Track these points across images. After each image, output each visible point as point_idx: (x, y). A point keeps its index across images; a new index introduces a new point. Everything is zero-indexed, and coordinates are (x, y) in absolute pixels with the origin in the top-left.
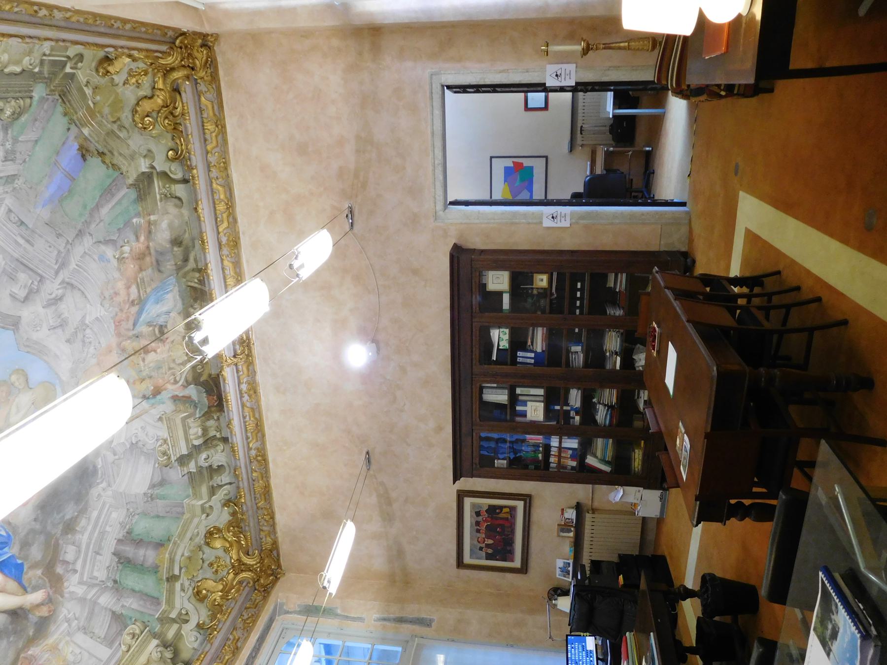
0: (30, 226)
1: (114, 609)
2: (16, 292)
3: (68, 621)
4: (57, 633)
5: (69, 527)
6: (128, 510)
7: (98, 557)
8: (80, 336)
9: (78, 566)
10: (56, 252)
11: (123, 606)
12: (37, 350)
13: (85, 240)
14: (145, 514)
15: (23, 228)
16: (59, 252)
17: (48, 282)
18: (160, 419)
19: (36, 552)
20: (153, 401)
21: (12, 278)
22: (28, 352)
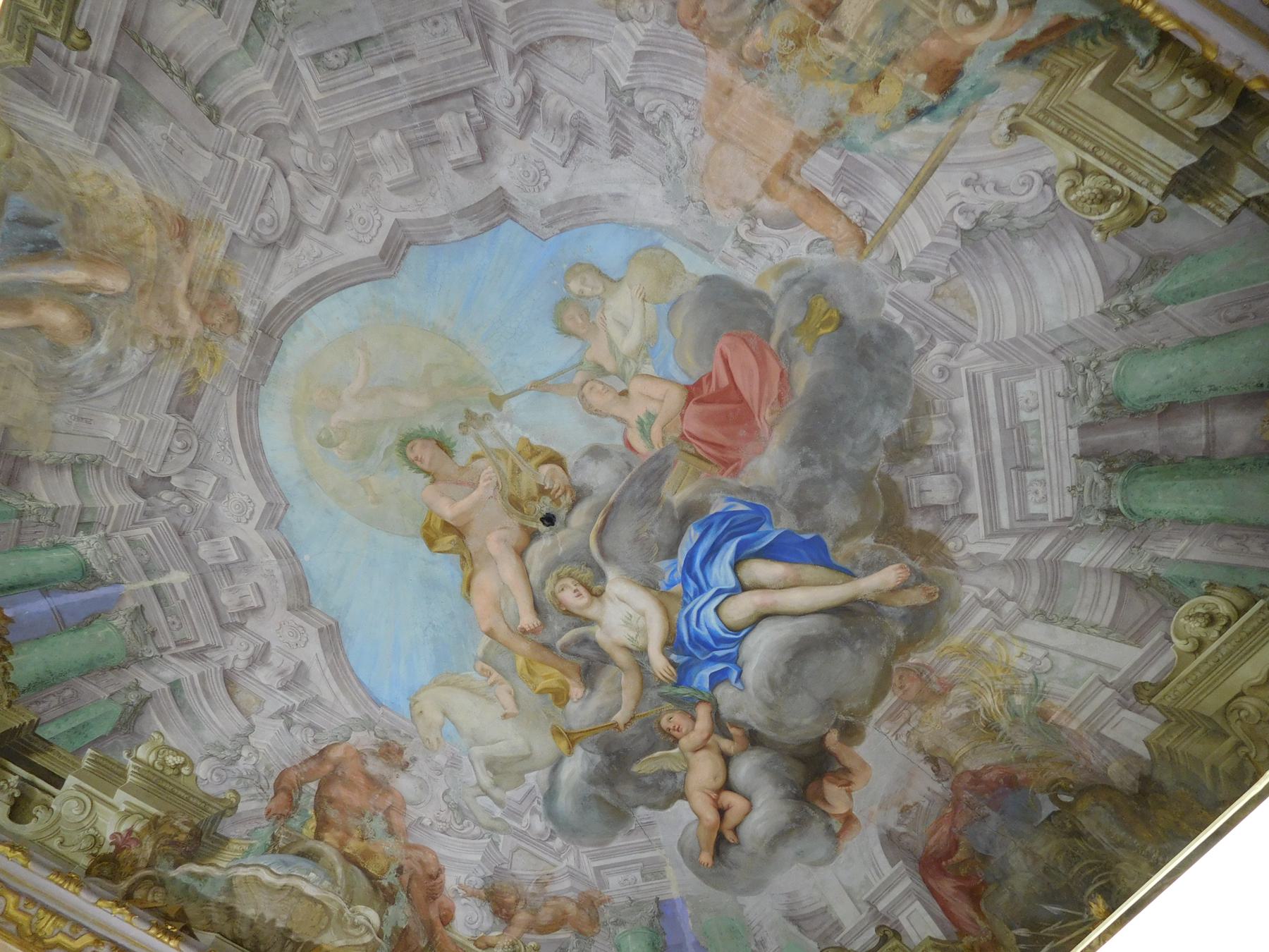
0: (377, 28)
1: (1126, 568)
2: (459, 156)
3: (989, 604)
4: (968, 625)
5: (906, 447)
6: (1067, 363)
7: (1029, 476)
8: (632, 123)
10: (452, 21)
11: (1155, 559)
12: (575, 213)
14: (1141, 351)
15: (368, 49)
17: (488, 87)
18: (1015, 130)
19: (840, 511)
20: (953, 105)
21: (435, 141)
22: (562, 231)
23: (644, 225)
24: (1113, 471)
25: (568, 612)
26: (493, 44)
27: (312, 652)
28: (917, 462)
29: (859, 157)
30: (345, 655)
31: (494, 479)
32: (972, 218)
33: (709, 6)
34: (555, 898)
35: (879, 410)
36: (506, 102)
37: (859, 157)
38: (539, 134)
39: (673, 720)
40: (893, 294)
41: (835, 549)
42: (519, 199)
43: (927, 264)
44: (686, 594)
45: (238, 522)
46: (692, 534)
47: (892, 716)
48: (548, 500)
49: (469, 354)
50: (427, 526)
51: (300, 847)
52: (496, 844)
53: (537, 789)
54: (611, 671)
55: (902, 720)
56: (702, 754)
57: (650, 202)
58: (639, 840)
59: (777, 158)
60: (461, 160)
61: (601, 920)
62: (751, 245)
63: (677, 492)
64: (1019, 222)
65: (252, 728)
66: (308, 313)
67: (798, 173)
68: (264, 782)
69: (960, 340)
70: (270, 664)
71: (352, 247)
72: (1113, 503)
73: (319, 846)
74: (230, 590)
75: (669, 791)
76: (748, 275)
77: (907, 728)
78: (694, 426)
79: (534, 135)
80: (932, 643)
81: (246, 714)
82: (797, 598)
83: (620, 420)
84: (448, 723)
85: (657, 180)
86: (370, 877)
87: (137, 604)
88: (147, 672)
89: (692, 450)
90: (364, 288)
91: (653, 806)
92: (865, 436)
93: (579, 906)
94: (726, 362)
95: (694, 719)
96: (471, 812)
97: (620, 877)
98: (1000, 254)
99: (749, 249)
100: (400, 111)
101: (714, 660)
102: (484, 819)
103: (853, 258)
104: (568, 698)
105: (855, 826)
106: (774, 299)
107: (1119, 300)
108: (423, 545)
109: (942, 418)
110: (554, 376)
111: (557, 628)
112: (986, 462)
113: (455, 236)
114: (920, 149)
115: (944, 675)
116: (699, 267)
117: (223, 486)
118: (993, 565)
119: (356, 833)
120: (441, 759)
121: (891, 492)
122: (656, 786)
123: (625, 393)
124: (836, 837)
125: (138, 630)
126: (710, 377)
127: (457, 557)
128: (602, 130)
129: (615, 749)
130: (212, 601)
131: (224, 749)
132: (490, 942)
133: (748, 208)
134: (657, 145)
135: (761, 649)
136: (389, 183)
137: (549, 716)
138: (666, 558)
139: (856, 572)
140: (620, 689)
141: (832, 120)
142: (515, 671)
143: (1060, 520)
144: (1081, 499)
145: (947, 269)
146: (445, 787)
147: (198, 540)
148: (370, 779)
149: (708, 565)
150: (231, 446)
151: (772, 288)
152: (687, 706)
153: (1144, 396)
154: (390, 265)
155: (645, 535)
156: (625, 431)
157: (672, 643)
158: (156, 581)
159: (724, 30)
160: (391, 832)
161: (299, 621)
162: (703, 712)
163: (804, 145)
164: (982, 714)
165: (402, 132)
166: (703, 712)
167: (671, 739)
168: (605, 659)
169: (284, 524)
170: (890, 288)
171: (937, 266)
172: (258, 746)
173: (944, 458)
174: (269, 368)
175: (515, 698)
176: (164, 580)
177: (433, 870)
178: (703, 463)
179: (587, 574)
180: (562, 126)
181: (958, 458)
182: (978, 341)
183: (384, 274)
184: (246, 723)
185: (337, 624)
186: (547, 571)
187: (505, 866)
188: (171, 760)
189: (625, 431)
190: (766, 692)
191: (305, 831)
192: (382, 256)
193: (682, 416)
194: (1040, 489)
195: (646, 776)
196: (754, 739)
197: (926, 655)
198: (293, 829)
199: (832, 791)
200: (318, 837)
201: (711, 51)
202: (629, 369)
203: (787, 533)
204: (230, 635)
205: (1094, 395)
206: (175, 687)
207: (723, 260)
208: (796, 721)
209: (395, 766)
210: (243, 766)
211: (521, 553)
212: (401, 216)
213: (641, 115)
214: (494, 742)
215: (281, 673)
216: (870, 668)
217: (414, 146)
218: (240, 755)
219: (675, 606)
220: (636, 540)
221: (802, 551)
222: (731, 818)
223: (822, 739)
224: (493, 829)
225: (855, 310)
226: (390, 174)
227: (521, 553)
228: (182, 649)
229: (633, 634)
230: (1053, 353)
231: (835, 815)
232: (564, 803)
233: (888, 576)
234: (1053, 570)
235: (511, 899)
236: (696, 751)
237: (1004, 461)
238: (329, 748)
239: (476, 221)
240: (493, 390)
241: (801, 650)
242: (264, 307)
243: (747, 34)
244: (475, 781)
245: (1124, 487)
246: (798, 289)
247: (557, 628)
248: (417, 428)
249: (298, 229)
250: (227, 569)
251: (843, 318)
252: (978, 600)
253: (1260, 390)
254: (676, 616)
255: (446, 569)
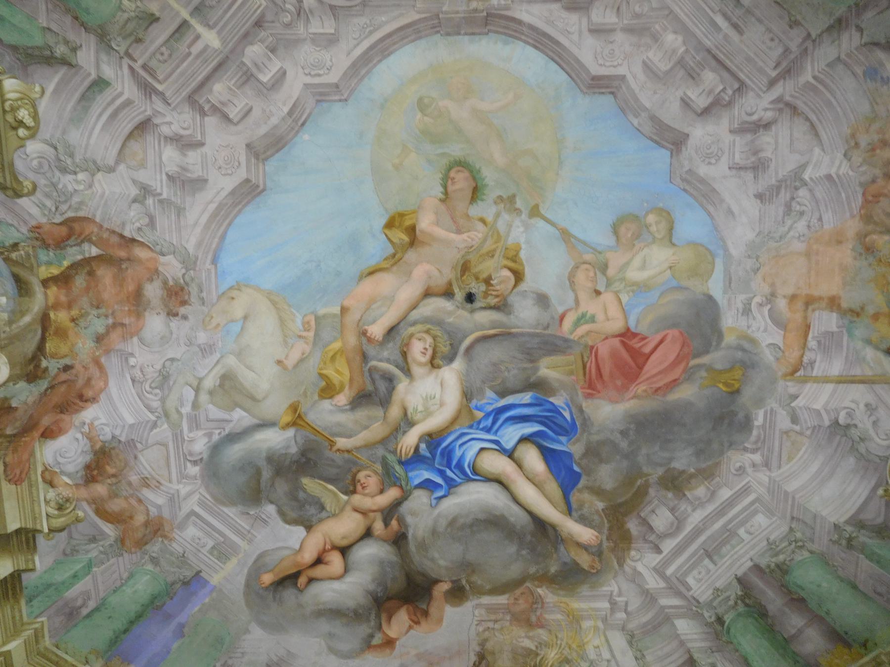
2: (693, 97)
3: (613, 604)
4: (588, 603)
5: (675, 483)
6: (791, 530)
7: (707, 561)
8: (784, 196)
9: (668, 546)
10: (780, 50)
12: (703, 193)
13: (845, 37)
14: (824, 560)
16: (787, 50)
17: (751, 94)
19: (607, 475)
21: (693, 76)
22: (685, 190)
23: (722, 239)
24: (743, 601)
25: (404, 355)
26: (781, 83)
27: (223, 184)
28: (670, 495)
29: (845, 338)
30: (240, 211)
31: (474, 243)
32: (849, 421)
33: (884, 202)
34: (140, 501)
35: (690, 451)
36: (749, 110)
37: (845, 338)
38: (740, 141)
39: (369, 479)
40: (772, 410)
41: (580, 491)
42: (689, 151)
43: (804, 416)
44: (479, 422)
45: (299, 71)
46: (526, 397)
47: (490, 609)
48: (483, 288)
49: (557, 174)
50: (402, 215)
51: (23, 273)
52: (155, 425)
53: (231, 425)
54: (379, 412)
55: (493, 617)
56: (358, 516)
57: (740, 234)
58: (244, 523)
59: (816, 293)
60: (692, 101)
61: (147, 547)
62: (750, 310)
63: (548, 369)
64: (862, 448)
65: (111, 170)
66: (521, 44)
67: (814, 310)
68: (64, 207)
69: (767, 464)
70: (185, 155)
71: (589, 53)
72: (726, 618)
73: (38, 289)
74: (230, 89)
75: (304, 514)
76: (730, 321)
77: (490, 625)
78: (604, 350)
79: (738, 139)
80: (562, 593)
81: (121, 156)
82: (528, 493)
83: (577, 302)
84: (240, 324)
85: (758, 230)
86: (41, 348)
87: (157, 14)
88: (97, 52)
89: (586, 359)
90: (564, 76)
91: (282, 513)
92: (666, 455)
93: (146, 524)
94: (661, 342)
95: (382, 492)
96: (170, 389)
97: (199, 534)
98: (836, 450)
99: (747, 311)
100: (700, 43)
101: (442, 473)
102: (171, 404)
103: (780, 374)
104: (331, 397)
105: (388, 651)
106: (723, 344)
107: (849, 529)
108: (383, 221)
109: (708, 489)
110: (579, 240)
111: (385, 354)
112: (697, 532)
113: (635, 122)
114: (871, 368)
115: (547, 616)
116: (715, 287)
117: (331, 41)
118: (639, 586)
119: (75, 312)
120: (202, 337)
121: (641, 494)
122: (302, 505)
123: (598, 293)
124: (368, 645)
125: (131, 26)
126: (644, 338)
127: (391, 250)
128: (769, 179)
129: (311, 456)
130: (208, 78)
131: (72, 156)
132: (56, 481)
133: (773, 295)
134: (780, 218)
135: (475, 496)
136: (647, 57)
137: (305, 394)
138: (496, 393)
139: (574, 514)
140: (366, 428)
141: (859, 310)
142: (325, 346)
143: (694, 598)
144: (715, 598)
145: (808, 428)
146: (178, 356)
147: (262, 41)
148: (138, 294)
149: (509, 423)
150: (371, 33)
151: (729, 339)
152: (388, 479)
153: (799, 582)
154: (590, 87)
155: (503, 368)
156: (570, 310)
157: (433, 439)
158: (193, 22)
159: (875, 218)
160: (99, 339)
161: (243, 159)
162: (393, 493)
163: (833, 303)
164: (539, 659)
165: (687, 51)
166: (393, 493)
167: (351, 488)
168: (385, 402)
169: (325, 105)
170: (775, 405)
171: (806, 422)
172: (96, 184)
173: (682, 509)
174: (459, 34)
175: (302, 360)
176: (200, 29)
177: (89, 393)
178: (581, 372)
179: (445, 349)
180: (756, 153)
181: (689, 516)
182: (773, 475)
183: (581, 85)
184: (111, 162)
185: (264, 190)
186: (426, 320)
187: (139, 445)
188: (23, 114)
189: (570, 310)
190: (443, 523)
191: (43, 269)
192: (594, 78)
193: (606, 338)
194: (703, 573)
195: (305, 491)
196: (399, 540)
197: (550, 595)
198: (36, 257)
199: (402, 617)
200: (45, 283)
201: (858, 218)
202: (617, 286)
203: (569, 455)
204: (187, 108)
205: (781, 557)
206: (100, 84)
207: (729, 300)
208: (436, 555)
209: (166, 306)
210: (67, 181)
211: (428, 294)
212: (629, 77)
213: (793, 199)
214: (249, 368)
215: (184, 169)
216: (515, 571)
217: (681, 63)
218: (75, 173)
219: (465, 421)
220: (495, 365)
221: (563, 473)
222: (319, 571)
223: (436, 582)
224: (167, 415)
225: (748, 394)
226: (654, 56)
227: (428, 294)
228: (142, 72)
229: (420, 408)
230: (793, 518)
231: (384, 633)
232: (235, 452)
233: (585, 534)
234: (662, 621)
235: (110, 470)
236: (356, 510)
237: (705, 541)
238: (142, 244)
239: (655, 131)
240: (541, 205)
241: (493, 522)
242: (507, 8)
243: (881, 233)
244: (202, 375)
245: (739, 615)
246: (739, 354)
247: (385, 354)
248: (478, 167)
249: (581, 8)
250: (248, 77)
251: (738, 391)
252: (611, 594)
253: (844, 635)
254: (457, 427)
255: (376, 248)
